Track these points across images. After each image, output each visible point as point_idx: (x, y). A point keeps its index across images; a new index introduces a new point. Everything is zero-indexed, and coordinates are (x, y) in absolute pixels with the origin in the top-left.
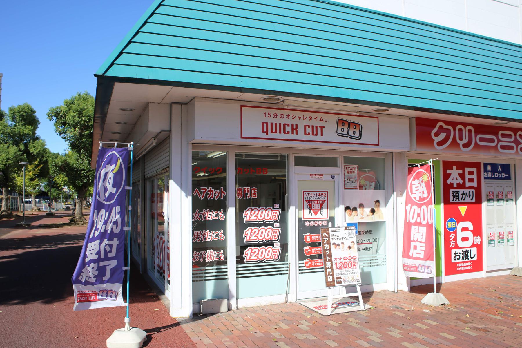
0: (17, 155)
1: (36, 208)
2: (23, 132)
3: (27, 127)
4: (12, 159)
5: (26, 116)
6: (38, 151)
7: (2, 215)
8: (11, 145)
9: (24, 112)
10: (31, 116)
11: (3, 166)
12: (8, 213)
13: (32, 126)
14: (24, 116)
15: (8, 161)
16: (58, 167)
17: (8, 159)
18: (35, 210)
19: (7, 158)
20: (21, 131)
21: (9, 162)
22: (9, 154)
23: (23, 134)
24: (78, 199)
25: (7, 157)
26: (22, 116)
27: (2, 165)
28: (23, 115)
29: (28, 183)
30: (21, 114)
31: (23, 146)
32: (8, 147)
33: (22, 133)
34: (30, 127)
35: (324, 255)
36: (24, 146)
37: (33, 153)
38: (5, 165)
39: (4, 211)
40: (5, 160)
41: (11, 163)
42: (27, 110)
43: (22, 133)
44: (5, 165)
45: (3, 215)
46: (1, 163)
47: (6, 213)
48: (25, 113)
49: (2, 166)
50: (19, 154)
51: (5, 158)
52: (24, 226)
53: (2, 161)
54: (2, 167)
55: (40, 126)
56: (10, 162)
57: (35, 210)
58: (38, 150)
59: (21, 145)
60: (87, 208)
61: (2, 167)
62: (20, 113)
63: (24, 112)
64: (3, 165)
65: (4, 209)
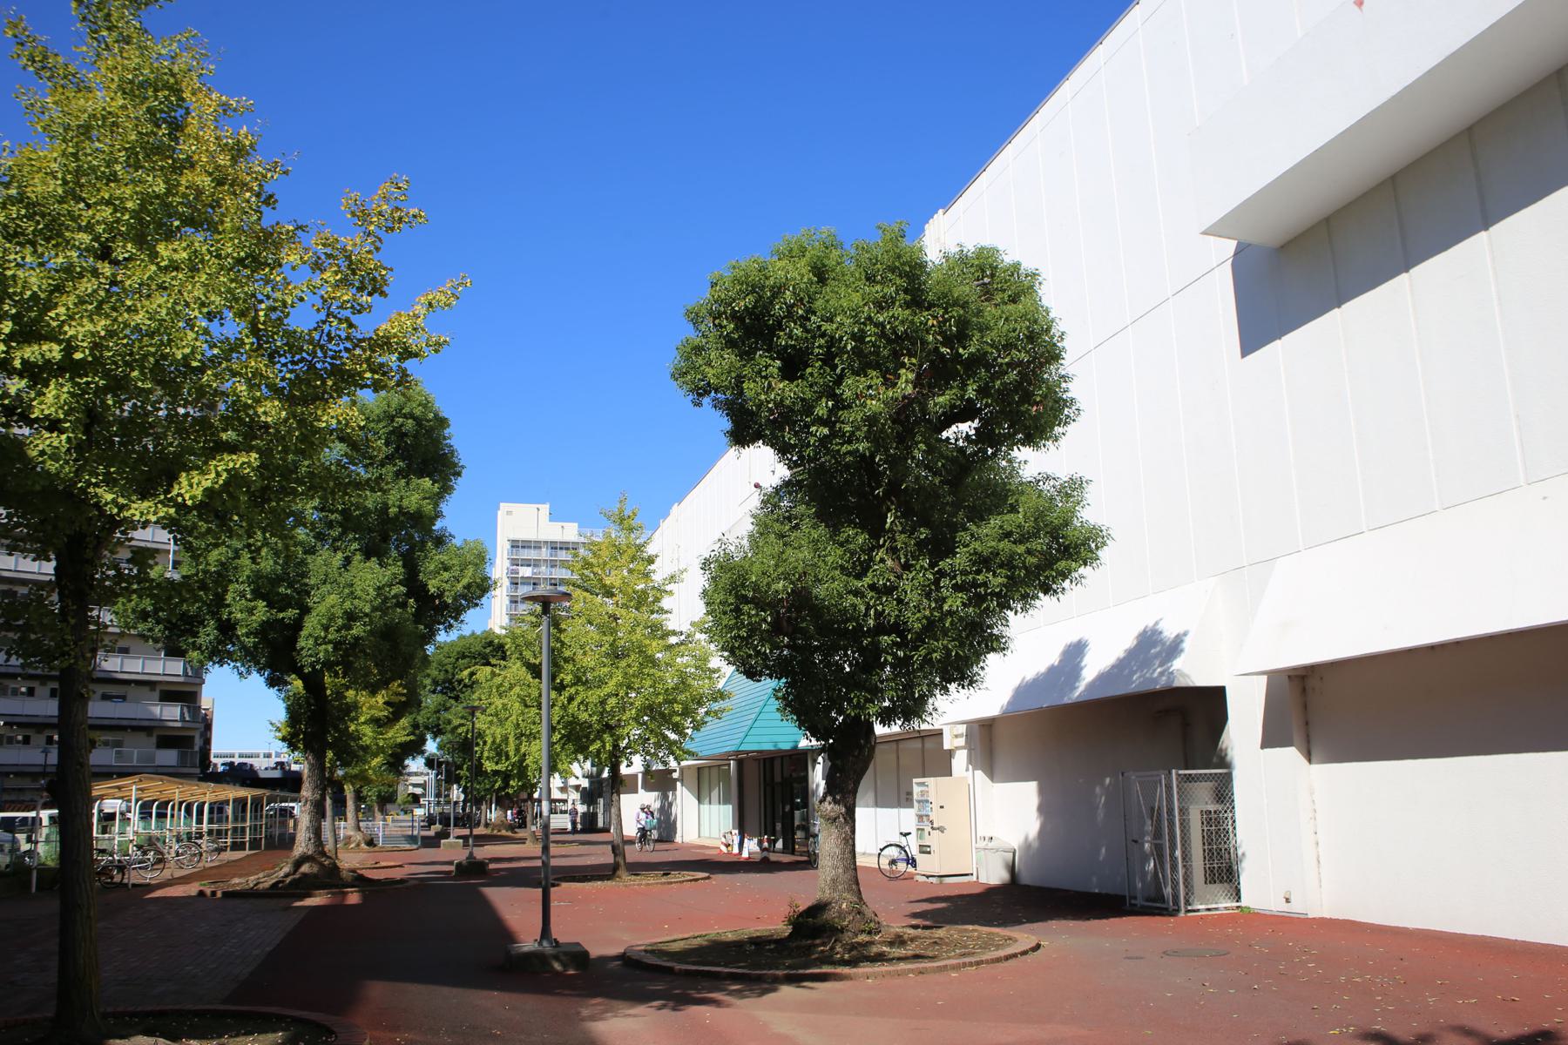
0: (386, 600)
1: (359, 837)
2: (400, 507)
3: (415, 481)
4: (366, 615)
5: (415, 437)
6: (464, 587)
7: (297, 876)
8: (358, 557)
9: (405, 416)
10: (430, 431)
11: (330, 647)
12: (321, 864)
13: (434, 482)
14: (405, 435)
15: (350, 628)
16: (773, 605)
17: (351, 617)
18: (358, 845)
19: (346, 612)
20: (390, 502)
21: (354, 632)
22: (352, 593)
23: (397, 516)
24: (835, 802)
25: (347, 605)
26: (398, 435)
27: (326, 643)
28: (403, 429)
29: (370, 738)
30: (395, 425)
31: (400, 563)
32: (347, 561)
33: (393, 511)
34: (427, 483)
35: (30, 820)
36: (404, 566)
37: (441, 595)
38: (337, 645)
39: (304, 859)
40: (340, 622)
41: (362, 634)
42: (418, 412)
43: (393, 511)
44: (337, 645)
45: (305, 875)
46: (322, 634)
47: (315, 869)
48: (410, 421)
49: (324, 646)
50: (393, 593)
51: (339, 613)
52: (557, 966)
53: (326, 628)
54: (326, 651)
55: (460, 485)
56: (358, 630)
57: (358, 845)
58: (465, 581)
59: (390, 561)
60: (509, 834)
61: (326, 651)
62: (393, 421)
63: (405, 416)
64: (330, 642)
65: (305, 850)
